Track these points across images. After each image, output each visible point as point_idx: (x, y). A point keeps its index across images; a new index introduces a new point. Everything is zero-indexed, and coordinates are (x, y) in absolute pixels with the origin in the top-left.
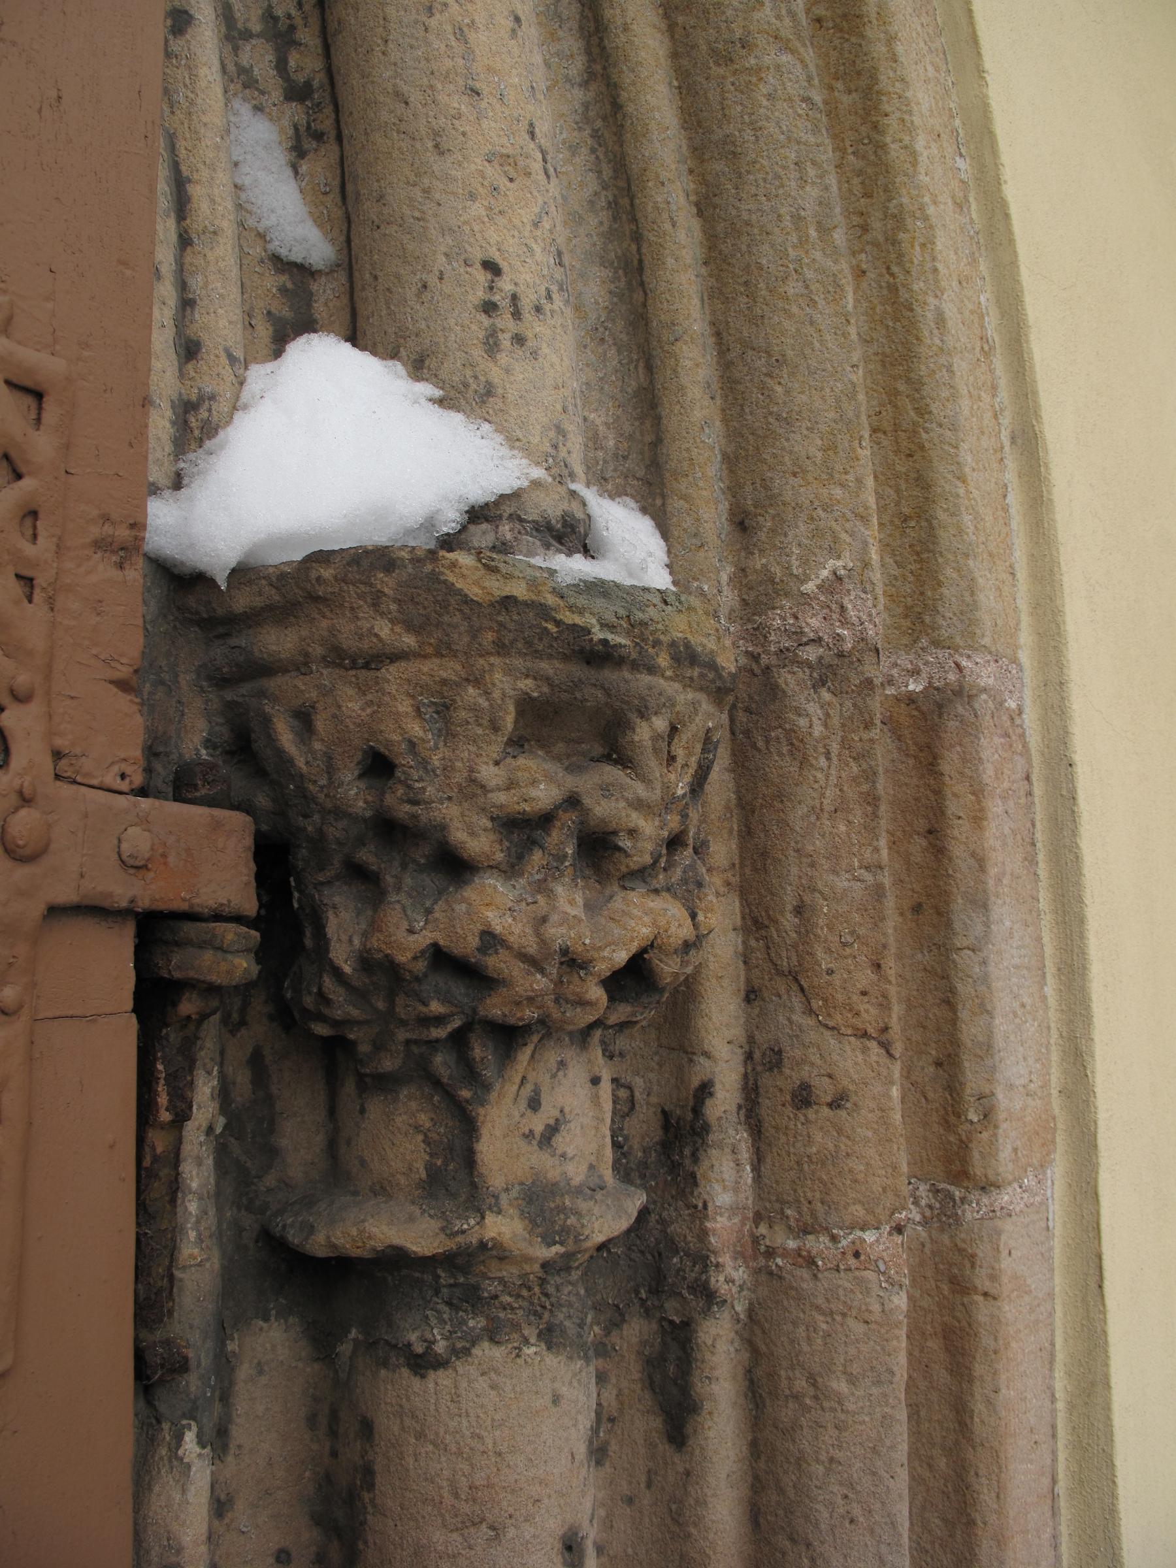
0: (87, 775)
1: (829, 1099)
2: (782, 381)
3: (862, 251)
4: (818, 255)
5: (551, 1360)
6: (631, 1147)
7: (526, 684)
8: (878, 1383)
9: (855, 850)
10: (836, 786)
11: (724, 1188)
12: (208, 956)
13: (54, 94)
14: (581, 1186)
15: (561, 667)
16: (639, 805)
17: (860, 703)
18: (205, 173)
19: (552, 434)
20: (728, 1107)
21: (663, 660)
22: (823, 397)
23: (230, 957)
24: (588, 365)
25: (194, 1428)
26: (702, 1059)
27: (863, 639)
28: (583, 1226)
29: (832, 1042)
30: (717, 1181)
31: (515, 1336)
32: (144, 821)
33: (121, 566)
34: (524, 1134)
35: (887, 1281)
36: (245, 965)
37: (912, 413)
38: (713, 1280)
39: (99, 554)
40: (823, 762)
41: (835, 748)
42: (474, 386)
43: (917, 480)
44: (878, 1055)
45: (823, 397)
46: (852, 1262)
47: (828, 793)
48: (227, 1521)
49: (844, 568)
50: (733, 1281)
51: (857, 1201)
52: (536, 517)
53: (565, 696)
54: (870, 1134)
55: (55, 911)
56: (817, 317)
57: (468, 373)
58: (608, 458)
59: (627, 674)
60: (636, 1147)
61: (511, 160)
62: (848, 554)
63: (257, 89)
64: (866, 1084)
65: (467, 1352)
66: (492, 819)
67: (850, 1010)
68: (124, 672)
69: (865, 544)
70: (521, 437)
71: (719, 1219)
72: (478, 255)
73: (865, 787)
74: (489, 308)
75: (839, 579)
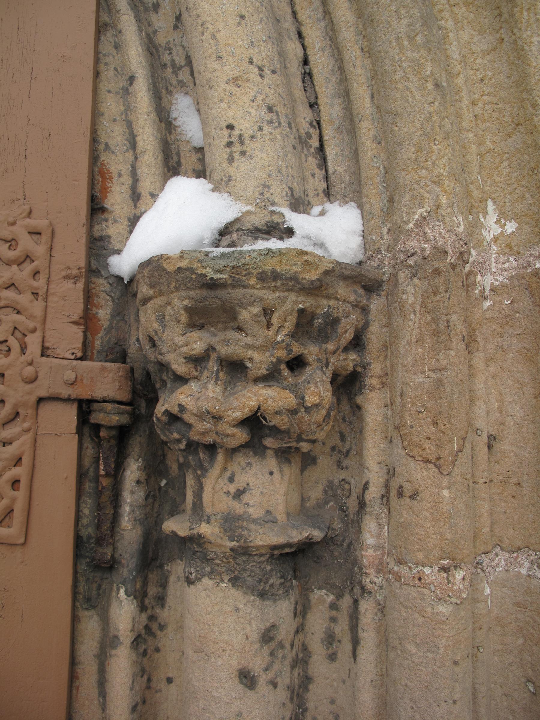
0: (58, 354)
1: (410, 494)
2: (398, 125)
3: (501, 28)
4: (409, 53)
5: (233, 591)
6: (349, 513)
7: (186, 302)
8: (431, 652)
9: (426, 361)
10: (418, 328)
11: (371, 535)
12: (102, 415)
13: (48, 134)
14: (257, 519)
15: (199, 292)
16: (249, 347)
17: (432, 283)
18: (141, 131)
19: (260, 189)
20: (375, 495)
21: (252, 281)
22: (414, 126)
23: (110, 416)
24: (336, 146)
25: (124, 588)
26: (366, 471)
27: (435, 247)
28: (250, 536)
29: (412, 464)
30: (368, 532)
31: (218, 577)
32: (73, 369)
33: (75, 283)
34: (225, 492)
35: (435, 597)
36: (117, 418)
37: (530, 109)
38: (363, 580)
39: (66, 280)
40: (412, 316)
41: (418, 308)
42: (224, 179)
43: (535, 146)
44: (434, 472)
45: (414, 126)
46: (417, 582)
47: (414, 332)
48: (164, 633)
49: (426, 211)
50: (375, 583)
51: (419, 550)
52: (249, 227)
53: (202, 304)
54: (428, 515)
55: (41, 400)
56: (410, 85)
57: (223, 174)
58: (347, 186)
59: (230, 290)
60: (351, 512)
61: (239, 78)
62: (427, 204)
63: (186, 86)
64: (427, 488)
65: (199, 579)
66: (185, 358)
67: (421, 447)
68: (75, 318)
69: (437, 196)
70: (243, 195)
71: (369, 550)
72: (224, 124)
73: (433, 327)
74: (229, 144)
75: (424, 218)
